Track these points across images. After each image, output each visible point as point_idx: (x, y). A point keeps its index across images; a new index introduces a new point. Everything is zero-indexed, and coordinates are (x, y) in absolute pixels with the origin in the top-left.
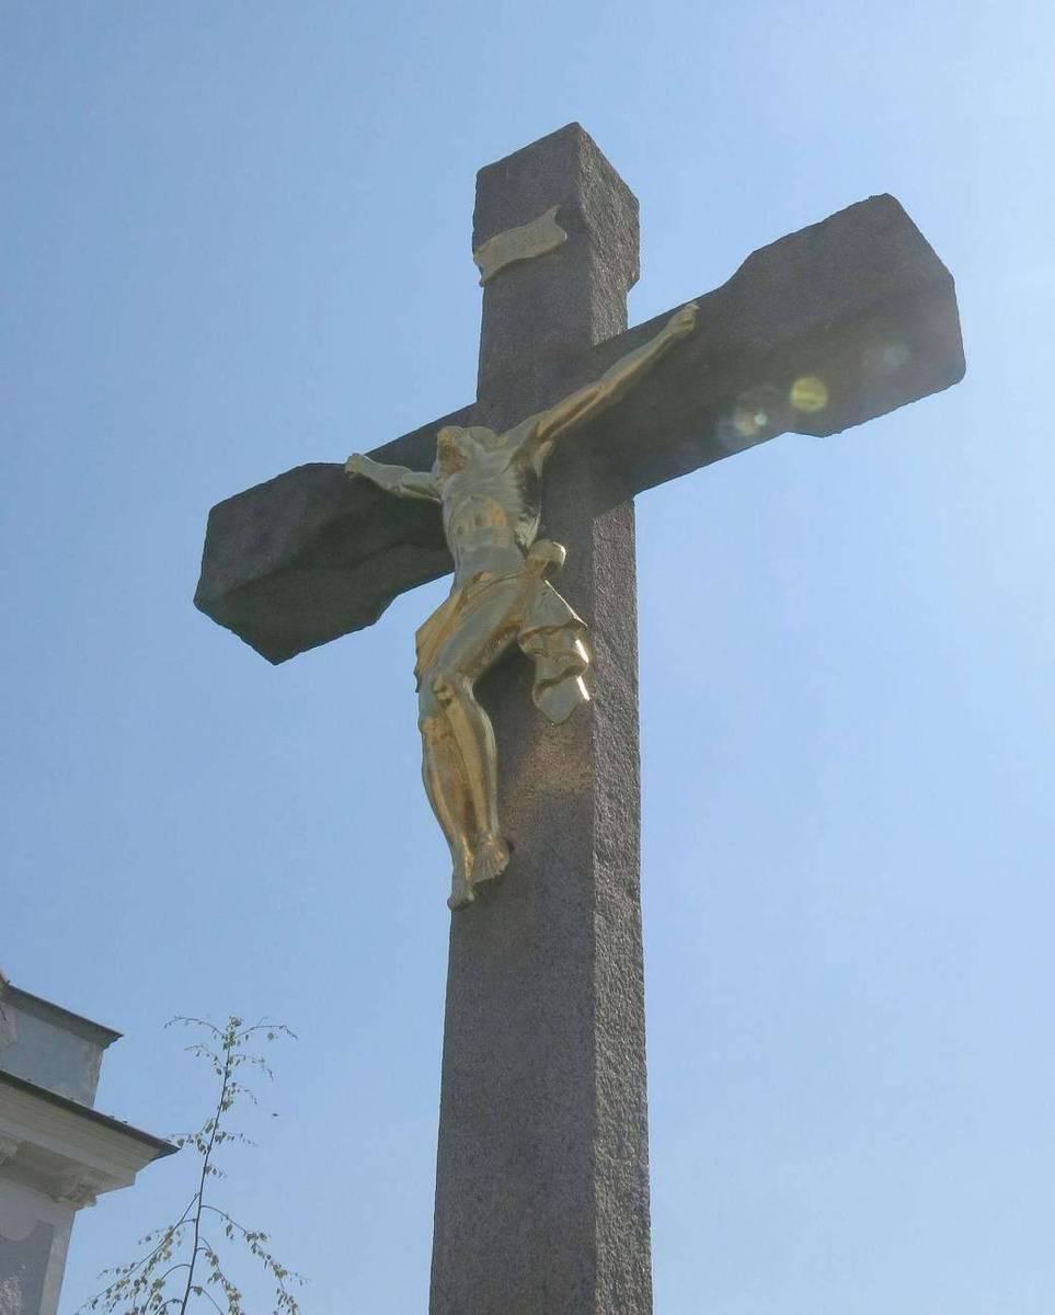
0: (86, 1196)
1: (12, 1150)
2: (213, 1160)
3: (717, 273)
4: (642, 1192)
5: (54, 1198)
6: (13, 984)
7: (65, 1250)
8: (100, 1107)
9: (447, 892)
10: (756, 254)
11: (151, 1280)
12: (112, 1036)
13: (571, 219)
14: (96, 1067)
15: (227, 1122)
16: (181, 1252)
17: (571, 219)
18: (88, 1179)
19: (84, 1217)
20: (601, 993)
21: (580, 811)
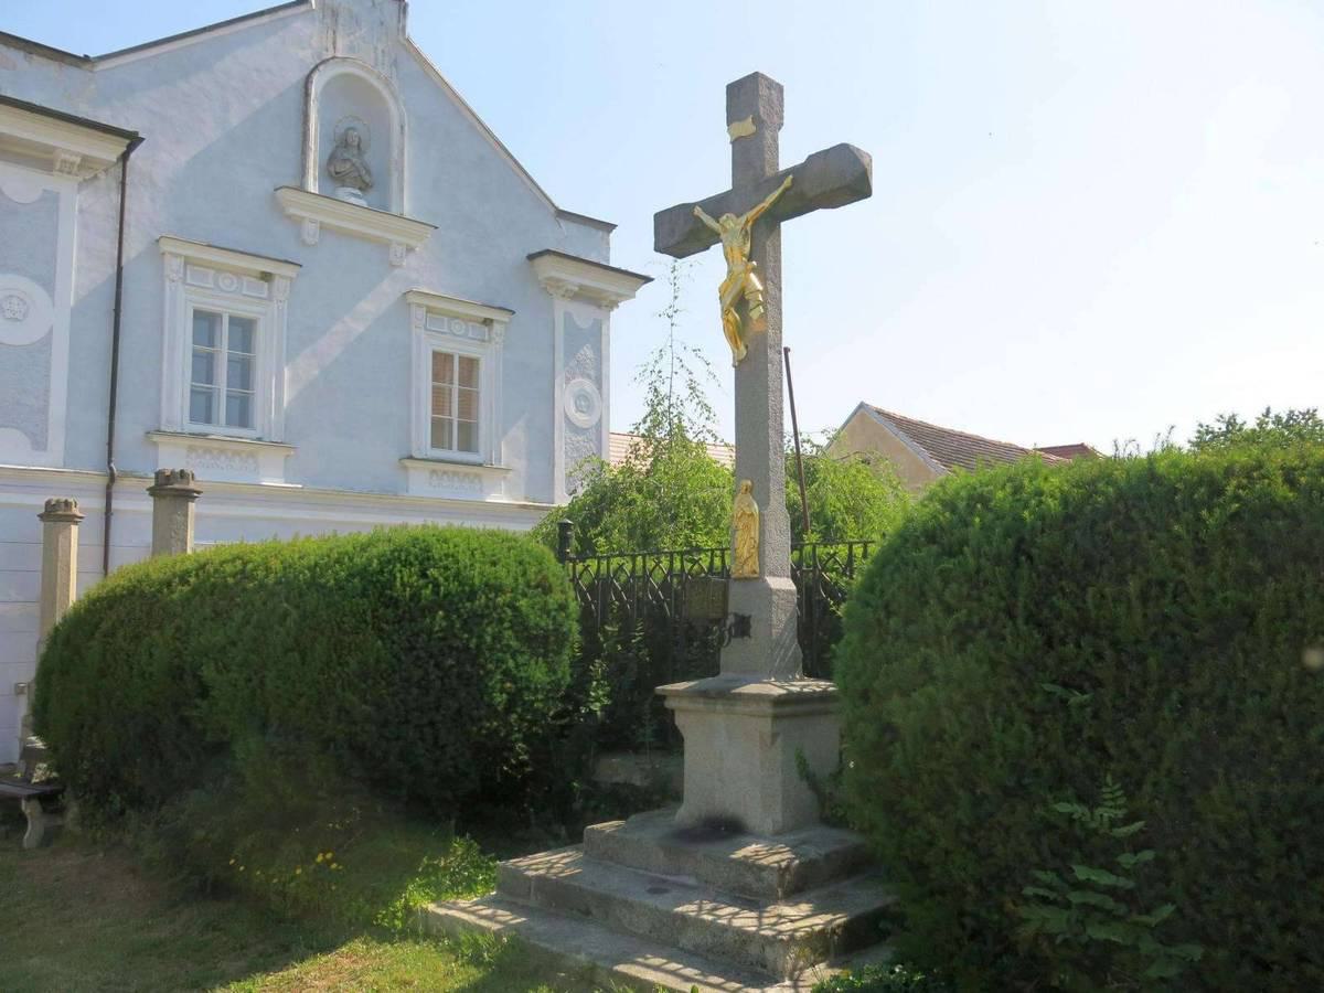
0: (614, 304)
1: (577, 289)
2: (674, 320)
3: (800, 159)
4: (476, 882)
5: (599, 307)
6: (561, 208)
7: (608, 329)
8: (612, 264)
9: (732, 362)
10: (810, 156)
11: (657, 370)
12: (614, 226)
13: (758, 121)
14: (608, 244)
15: (678, 304)
16: (667, 358)
17: (758, 121)
18: (613, 298)
19: (614, 314)
20: (770, 384)
21: (764, 335)
